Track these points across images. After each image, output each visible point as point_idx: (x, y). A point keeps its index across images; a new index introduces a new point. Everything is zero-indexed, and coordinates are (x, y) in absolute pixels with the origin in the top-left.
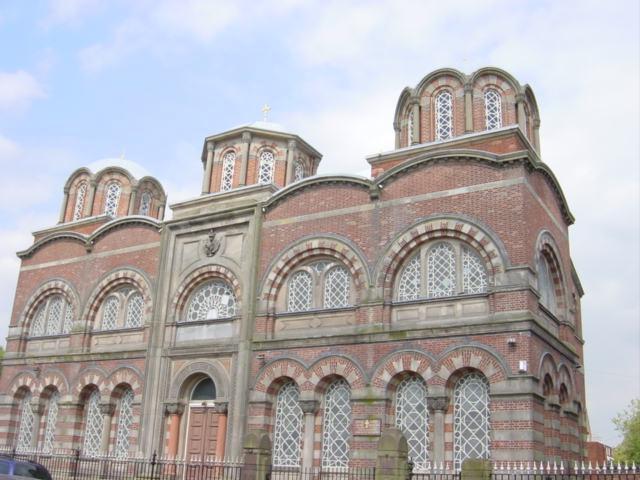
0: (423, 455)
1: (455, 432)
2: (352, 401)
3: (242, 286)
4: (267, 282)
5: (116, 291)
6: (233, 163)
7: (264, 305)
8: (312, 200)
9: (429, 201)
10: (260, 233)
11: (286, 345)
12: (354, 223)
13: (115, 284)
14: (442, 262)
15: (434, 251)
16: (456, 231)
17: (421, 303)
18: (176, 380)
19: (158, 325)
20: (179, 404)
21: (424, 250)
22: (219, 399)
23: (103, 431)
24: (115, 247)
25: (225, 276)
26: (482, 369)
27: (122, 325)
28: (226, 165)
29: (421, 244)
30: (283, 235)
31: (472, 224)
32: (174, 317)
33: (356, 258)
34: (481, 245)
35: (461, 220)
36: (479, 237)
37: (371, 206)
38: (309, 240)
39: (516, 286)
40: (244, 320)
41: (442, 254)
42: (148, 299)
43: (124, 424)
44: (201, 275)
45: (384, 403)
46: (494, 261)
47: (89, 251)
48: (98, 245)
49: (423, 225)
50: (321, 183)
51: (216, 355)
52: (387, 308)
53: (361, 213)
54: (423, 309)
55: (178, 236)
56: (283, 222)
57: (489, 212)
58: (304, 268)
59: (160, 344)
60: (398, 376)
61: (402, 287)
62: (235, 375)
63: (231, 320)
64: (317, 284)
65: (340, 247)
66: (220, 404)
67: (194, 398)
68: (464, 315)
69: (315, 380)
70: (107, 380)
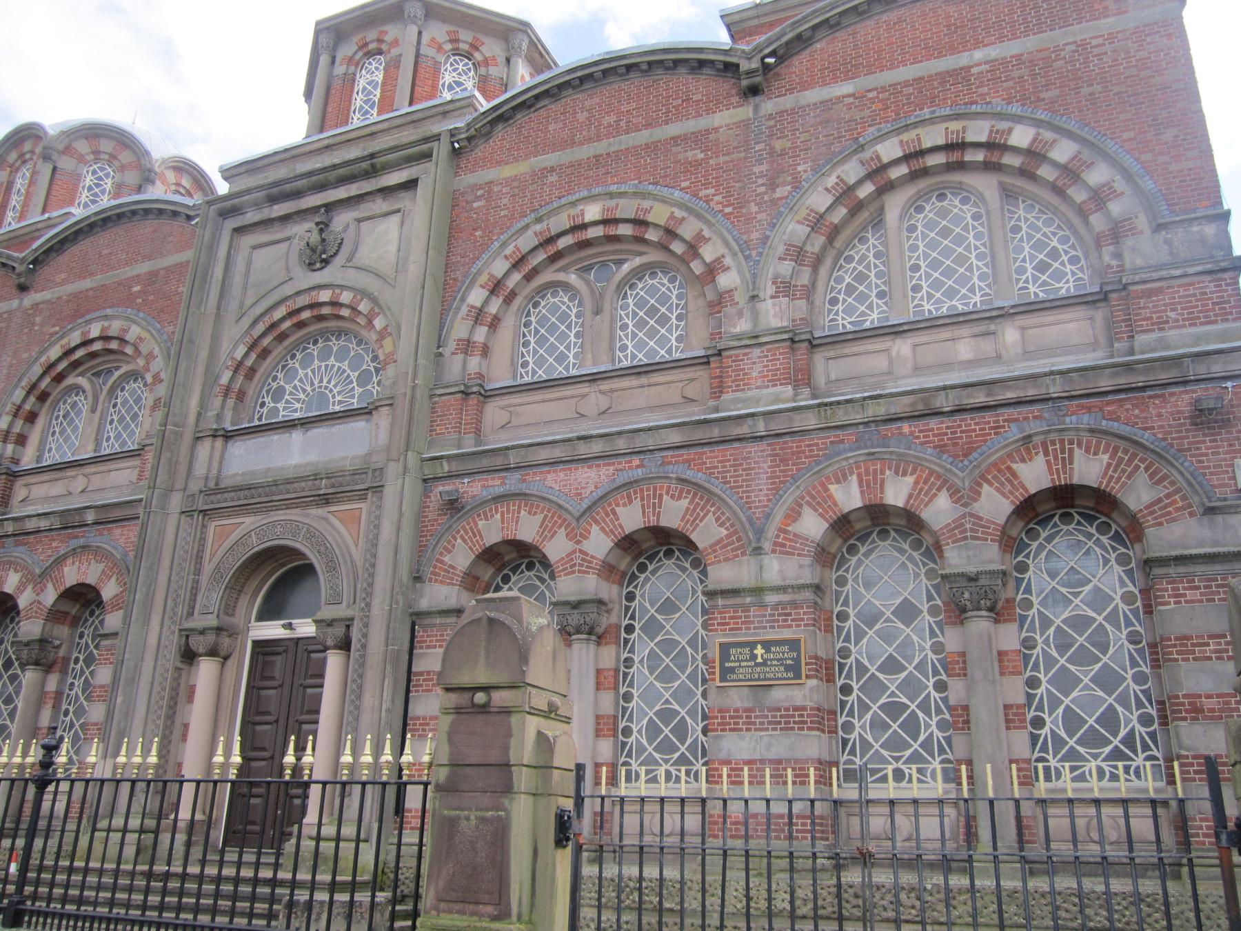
0: (692, 748)
1: (622, 690)
2: (711, 594)
3: (399, 328)
4: (464, 309)
5: (82, 374)
6: (379, 77)
7: (455, 367)
8: (582, 117)
9: (906, 84)
10: (455, 202)
11: (513, 459)
12: (778, 145)
13: (79, 354)
14: (945, 233)
15: (919, 209)
16: (989, 146)
17: (896, 331)
18: (218, 568)
19: (179, 436)
20: (219, 630)
21: (894, 205)
22: (327, 613)
23: (20, 703)
24: (84, 273)
25: (354, 309)
26: (1115, 489)
27: (91, 447)
28: (361, 83)
29: (887, 188)
30: (505, 201)
31: (1038, 123)
32: (219, 417)
33: (706, 233)
34: (1071, 172)
35: (1000, 116)
36: (1063, 151)
37: (745, 112)
38: (573, 204)
39: (1193, 262)
40: (403, 406)
41: (943, 213)
42: (157, 379)
43: (77, 690)
44: (291, 314)
45: (808, 595)
46: (1115, 208)
47: (23, 288)
48: (45, 272)
49: (895, 141)
50: (605, 72)
51: (325, 500)
52: (473, 400)
53: (716, 129)
54: (902, 347)
55: (239, 230)
56: (508, 171)
57: (1086, 90)
58: (561, 277)
59: (179, 484)
60: (842, 525)
61: (834, 301)
62: (374, 544)
63: (366, 412)
64: (598, 311)
65: (659, 214)
66: (330, 623)
67: (262, 617)
68: (1027, 354)
69: (599, 544)
70: (38, 581)
